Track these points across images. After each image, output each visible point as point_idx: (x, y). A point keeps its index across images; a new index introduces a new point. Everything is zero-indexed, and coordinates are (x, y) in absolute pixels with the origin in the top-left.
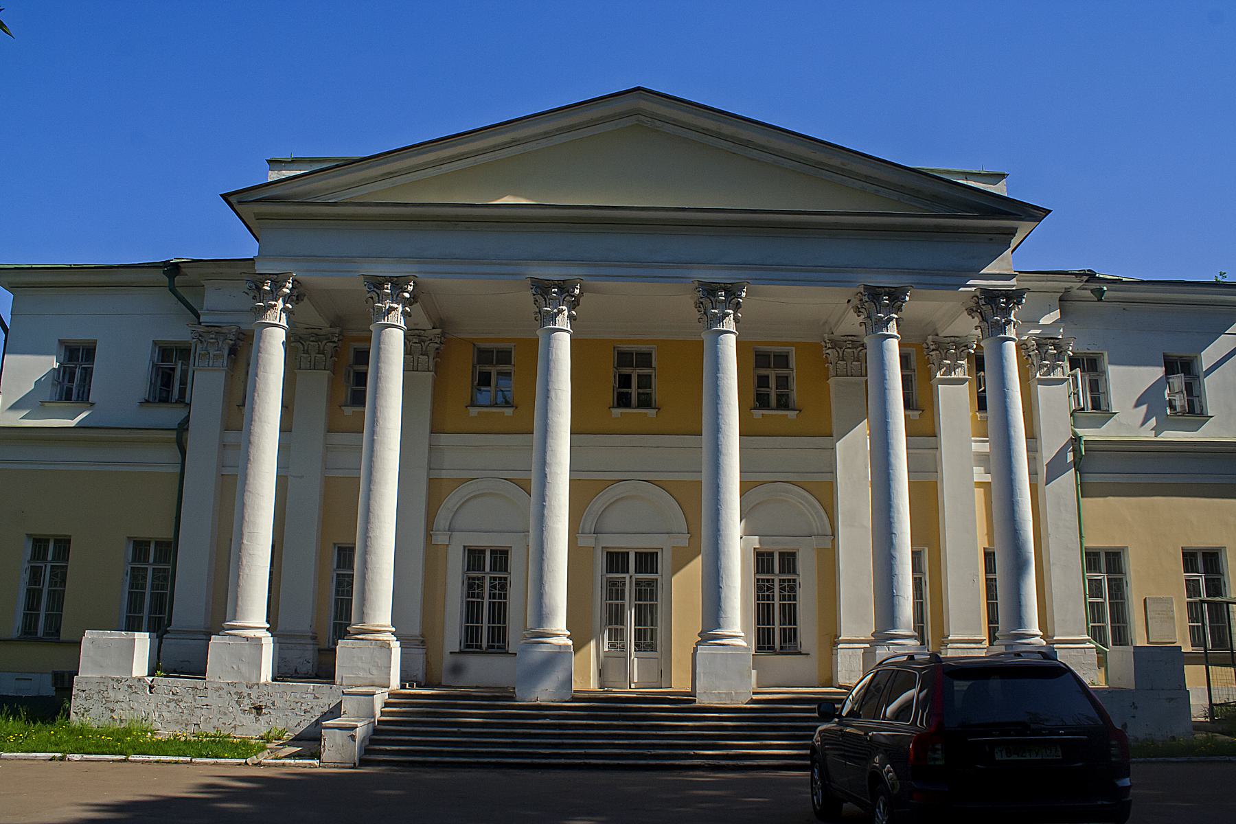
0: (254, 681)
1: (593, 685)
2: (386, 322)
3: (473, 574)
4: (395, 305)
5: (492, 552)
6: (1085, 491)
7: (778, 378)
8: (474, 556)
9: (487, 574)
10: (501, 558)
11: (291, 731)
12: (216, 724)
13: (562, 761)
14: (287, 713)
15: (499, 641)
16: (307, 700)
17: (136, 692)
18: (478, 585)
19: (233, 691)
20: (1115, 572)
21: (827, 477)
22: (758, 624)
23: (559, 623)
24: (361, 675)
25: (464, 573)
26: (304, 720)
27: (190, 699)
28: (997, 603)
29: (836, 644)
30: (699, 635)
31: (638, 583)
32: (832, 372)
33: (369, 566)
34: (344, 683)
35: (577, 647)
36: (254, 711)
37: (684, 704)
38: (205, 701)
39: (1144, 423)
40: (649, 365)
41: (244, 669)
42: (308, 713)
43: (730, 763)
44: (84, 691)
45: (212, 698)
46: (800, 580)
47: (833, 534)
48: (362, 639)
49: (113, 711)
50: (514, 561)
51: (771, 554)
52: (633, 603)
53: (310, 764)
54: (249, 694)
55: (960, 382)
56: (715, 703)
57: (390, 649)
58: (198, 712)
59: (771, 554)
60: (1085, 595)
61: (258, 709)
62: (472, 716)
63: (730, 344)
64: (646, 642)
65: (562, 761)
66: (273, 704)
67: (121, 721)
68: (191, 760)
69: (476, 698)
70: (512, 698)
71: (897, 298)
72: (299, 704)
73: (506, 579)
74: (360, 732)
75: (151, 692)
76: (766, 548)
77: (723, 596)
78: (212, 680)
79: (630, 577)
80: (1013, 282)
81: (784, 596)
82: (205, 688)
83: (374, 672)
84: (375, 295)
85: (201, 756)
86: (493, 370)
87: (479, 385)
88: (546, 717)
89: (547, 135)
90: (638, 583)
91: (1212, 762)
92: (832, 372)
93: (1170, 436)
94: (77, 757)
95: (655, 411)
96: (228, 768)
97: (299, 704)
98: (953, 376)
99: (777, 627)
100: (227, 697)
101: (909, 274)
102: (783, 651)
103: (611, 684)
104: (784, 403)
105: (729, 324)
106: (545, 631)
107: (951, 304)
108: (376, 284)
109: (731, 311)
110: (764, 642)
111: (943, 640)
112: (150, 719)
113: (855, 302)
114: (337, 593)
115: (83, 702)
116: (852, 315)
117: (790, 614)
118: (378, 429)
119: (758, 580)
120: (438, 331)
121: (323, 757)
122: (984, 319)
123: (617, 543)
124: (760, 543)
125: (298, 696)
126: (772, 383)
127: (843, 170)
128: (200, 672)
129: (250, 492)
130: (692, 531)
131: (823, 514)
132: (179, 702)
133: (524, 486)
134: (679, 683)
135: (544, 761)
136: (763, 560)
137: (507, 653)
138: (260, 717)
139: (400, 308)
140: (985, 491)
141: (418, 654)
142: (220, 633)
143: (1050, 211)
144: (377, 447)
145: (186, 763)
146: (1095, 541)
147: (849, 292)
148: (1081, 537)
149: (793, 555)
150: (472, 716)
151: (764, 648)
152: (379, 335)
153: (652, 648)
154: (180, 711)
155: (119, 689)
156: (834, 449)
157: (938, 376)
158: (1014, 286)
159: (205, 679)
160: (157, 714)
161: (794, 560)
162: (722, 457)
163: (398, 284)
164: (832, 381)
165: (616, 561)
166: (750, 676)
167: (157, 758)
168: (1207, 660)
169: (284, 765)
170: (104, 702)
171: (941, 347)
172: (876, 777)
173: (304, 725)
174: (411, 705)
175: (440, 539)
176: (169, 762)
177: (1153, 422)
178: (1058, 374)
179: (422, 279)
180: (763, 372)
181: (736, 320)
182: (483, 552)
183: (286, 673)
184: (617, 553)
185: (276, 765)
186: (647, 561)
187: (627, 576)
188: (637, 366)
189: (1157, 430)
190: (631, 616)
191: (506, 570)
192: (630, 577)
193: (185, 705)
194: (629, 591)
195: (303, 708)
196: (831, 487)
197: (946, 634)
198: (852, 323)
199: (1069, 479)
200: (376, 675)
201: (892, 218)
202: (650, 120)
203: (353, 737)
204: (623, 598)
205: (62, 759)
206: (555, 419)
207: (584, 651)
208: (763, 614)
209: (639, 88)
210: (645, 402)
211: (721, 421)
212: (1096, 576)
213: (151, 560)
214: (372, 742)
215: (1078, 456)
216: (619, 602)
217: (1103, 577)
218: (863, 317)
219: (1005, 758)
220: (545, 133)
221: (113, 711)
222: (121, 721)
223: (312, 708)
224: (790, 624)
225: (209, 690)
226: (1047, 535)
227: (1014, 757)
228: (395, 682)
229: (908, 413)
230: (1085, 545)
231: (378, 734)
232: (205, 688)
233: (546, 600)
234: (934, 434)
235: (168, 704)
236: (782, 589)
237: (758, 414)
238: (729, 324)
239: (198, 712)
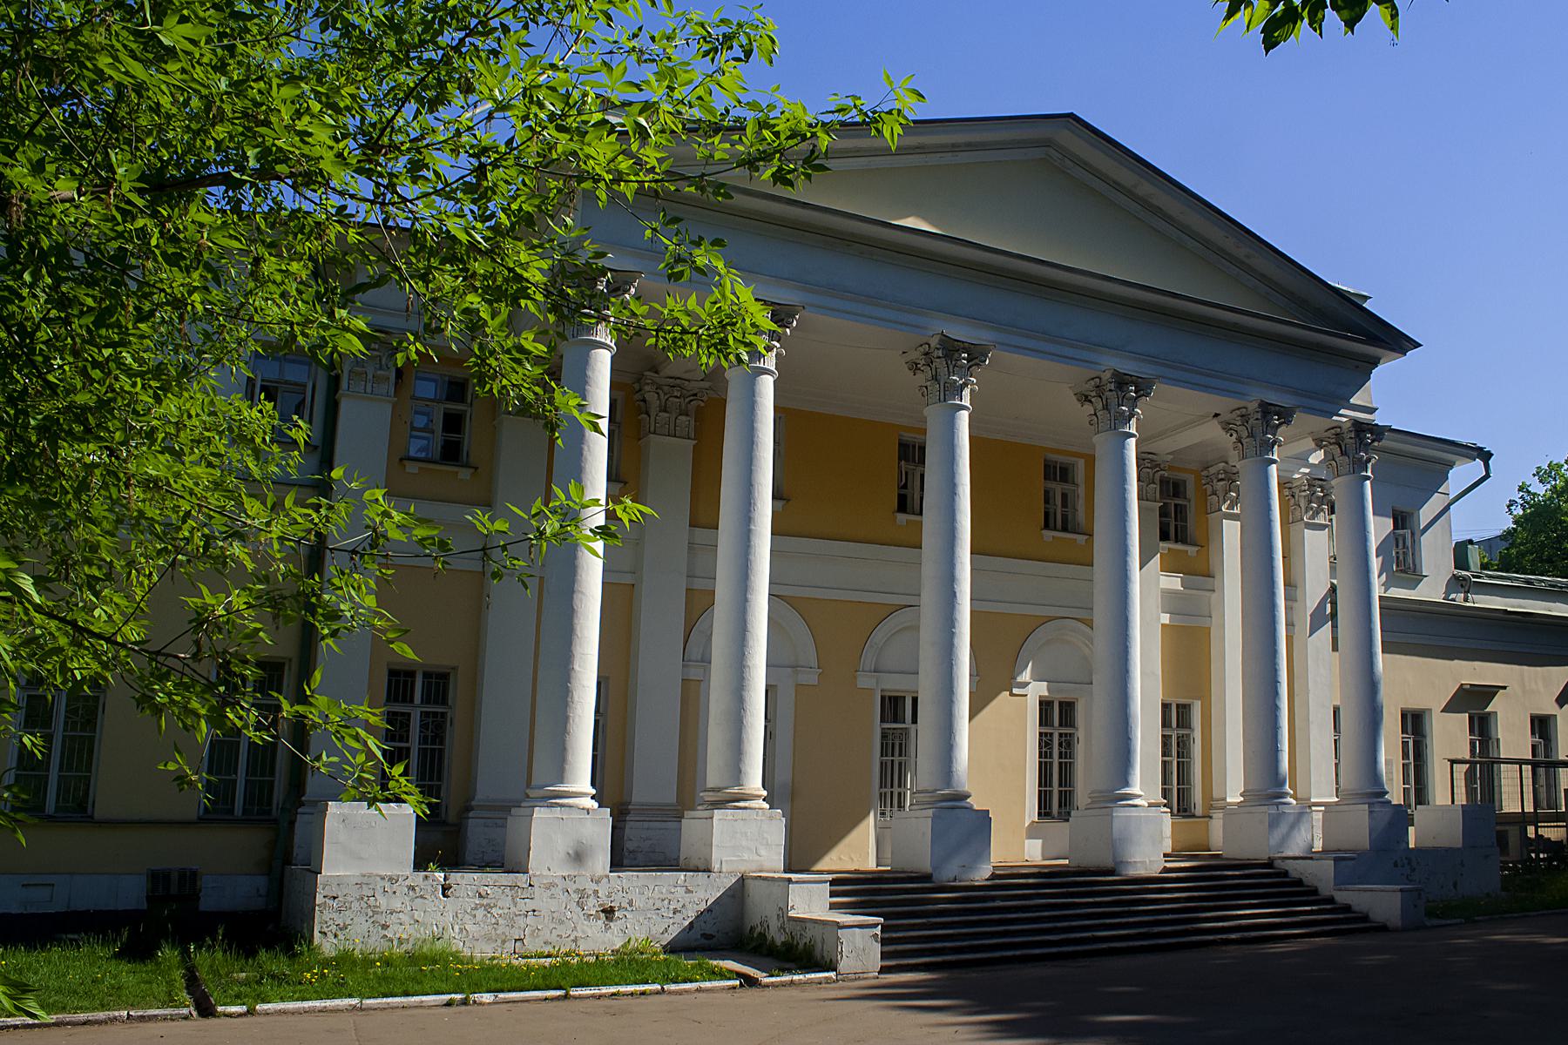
2: (762, 365)
5: (427, 675)
10: (438, 684)
12: (548, 937)
14: (649, 916)
16: (677, 895)
17: (422, 897)
18: (427, 729)
19: (572, 887)
24: (746, 857)
26: (673, 924)
27: (507, 902)
34: (724, 870)
36: (602, 915)
38: (530, 905)
42: (678, 914)
44: (335, 898)
45: (542, 901)
48: (745, 808)
49: (385, 927)
53: (826, 978)
54: (596, 892)
58: (521, 922)
61: (609, 912)
66: (631, 903)
68: (663, 988)
72: (666, 902)
75: (444, 895)
78: (538, 873)
82: (530, 885)
88: (993, 899)
89: (954, 148)
90: (425, 714)
94: (487, 998)
97: (666, 902)
100: (563, 897)
106: (747, 792)
112: (446, 936)
115: (335, 915)
125: (664, 891)
129: (582, 593)
132: (491, 908)
135: (1054, 950)
136: (398, 682)
138: (611, 924)
142: (523, 805)
143: (1420, 345)
145: (657, 993)
154: (494, 921)
155: (395, 893)
160: (457, 928)
167: (613, 989)
170: (371, 914)
178: (1321, 520)
183: (495, 862)
193: (500, 912)
195: (671, 907)
201: (1308, 332)
202: (1060, 156)
205: (465, 1002)
209: (1071, 116)
220: (953, 145)
221: (385, 927)
223: (684, 906)
225: (536, 889)
232: (530, 885)
235: (474, 912)
239: (521, 921)
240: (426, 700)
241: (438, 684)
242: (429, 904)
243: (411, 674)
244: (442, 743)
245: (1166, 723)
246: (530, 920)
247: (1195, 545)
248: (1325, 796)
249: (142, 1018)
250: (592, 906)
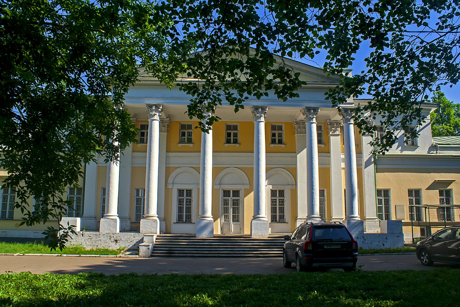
0: (115, 232)
1: (219, 233)
3: (180, 198)
4: (156, 113)
5: (187, 191)
6: (377, 170)
7: (279, 134)
8: (181, 192)
9: (185, 197)
10: (189, 192)
11: (127, 247)
12: (103, 246)
13: (212, 255)
15: (189, 219)
20: (386, 197)
21: (294, 166)
23: (209, 213)
25: (177, 197)
29: (297, 219)
30: (253, 217)
31: (233, 200)
32: (296, 132)
33: (150, 196)
35: (214, 221)
37: (248, 238)
38: (99, 239)
39: (397, 149)
40: (237, 130)
41: (111, 229)
43: (262, 255)
45: (102, 238)
46: (285, 199)
47: (296, 185)
50: (194, 194)
51: (276, 191)
52: (232, 206)
54: (113, 236)
55: (338, 135)
56: (257, 238)
57: (157, 222)
59: (276, 191)
60: (376, 204)
61: (116, 241)
62: (183, 242)
63: (262, 126)
64: (236, 219)
65: (212, 255)
66: (121, 239)
67: (73, 245)
69: (184, 237)
70: (195, 237)
71: (316, 111)
73: (191, 199)
74: (150, 247)
76: (274, 189)
77: (260, 205)
79: (231, 199)
80: (353, 105)
81: (187, 204)
83: (152, 229)
84: (149, 110)
85: (103, 255)
86: (186, 131)
87: (182, 136)
92: (296, 132)
93: (406, 153)
94: (65, 255)
96: (111, 257)
98: (335, 133)
99: (278, 214)
100: (106, 237)
101: (320, 102)
102: (280, 222)
103: (225, 233)
104: (280, 142)
105: (262, 119)
107: (333, 112)
108: (150, 106)
109: (263, 115)
110: (274, 219)
111: (330, 217)
113: (303, 111)
114: (136, 205)
116: (302, 115)
117: (282, 210)
118: (152, 153)
119: (272, 199)
120: (168, 119)
121: (140, 254)
122: (344, 117)
123: (227, 187)
124: (272, 187)
126: (277, 135)
127: (299, 69)
128: (98, 229)
130: (251, 184)
131: (292, 177)
133: (198, 170)
134: (247, 232)
137: (192, 223)
139: (158, 114)
140: (345, 171)
141: (164, 223)
144: (152, 159)
145: (98, 257)
146: (381, 187)
147: (301, 108)
148: (375, 185)
149: (283, 191)
150: (183, 242)
151: (273, 221)
152: (151, 123)
153: (238, 221)
156: (296, 157)
157: (331, 133)
158: (353, 107)
161: (419, 193)
162: (260, 161)
163: (157, 106)
164: (296, 135)
165: (226, 193)
166: (268, 229)
167: (89, 255)
168: (412, 224)
169: (128, 257)
171: (332, 124)
172: (297, 254)
173: (131, 246)
174: (164, 239)
175: (170, 186)
176: (93, 257)
177: (400, 148)
179: (165, 104)
180: (274, 132)
181: (265, 117)
184: (227, 191)
185: (126, 257)
186: (236, 193)
187: (230, 198)
188: (233, 130)
189: (402, 151)
190: (231, 211)
191: (191, 196)
192: (231, 199)
194: (230, 203)
196: (296, 169)
197: (365, 216)
198: (302, 117)
199: (372, 166)
200: (153, 230)
203: (149, 248)
204: (228, 205)
205: (61, 256)
206: (208, 150)
207: (216, 222)
208: (273, 210)
210: (236, 142)
211: (260, 150)
212: (380, 198)
213: (75, 194)
214: (153, 250)
215: (375, 159)
216: (227, 206)
217: (383, 198)
218: (305, 116)
219: (327, 248)
222: (73, 245)
224: (282, 213)
226: (365, 185)
227: (329, 248)
228: (158, 233)
229: (319, 145)
230: (377, 188)
231: (155, 247)
233: (205, 206)
234: (329, 152)
236: (279, 202)
237: (272, 145)
238: (262, 119)
239: (97, 242)
240: (187, 196)
241: (189, 192)
242: (79, 238)
243: (381, 191)
244: (283, 205)
245: (272, 195)
246: (99, 242)
247: (324, 144)
248: (372, 216)
249: (6, 255)
250: (112, 239)
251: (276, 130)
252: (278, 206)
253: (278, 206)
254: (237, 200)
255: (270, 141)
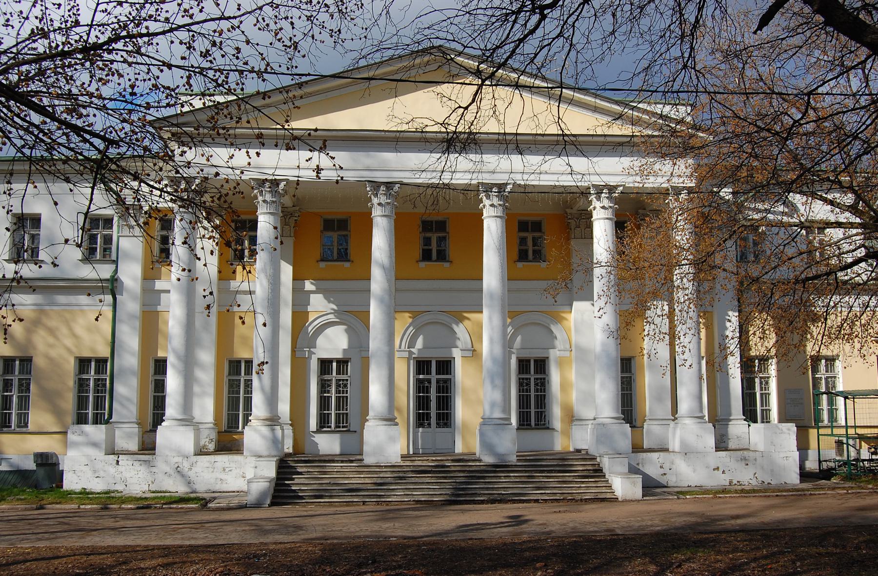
22: (520, 408)
25: (318, 377)
28: (347, 397)
73: (544, 379)
81: (537, 389)
91: (746, 497)
95: (448, 263)
126: (530, 242)
136: (523, 365)
159: (154, 454)
161: (544, 365)
174: (526, 471)
182: (528, 361)
188: (436, 231)
191: (545, 373)
224: (628, 407)
237: (520, 265)
251: (528, 231)
252: (533, 394)
253: (533, 394)
254: (249, 380)
255: (515, 255)
